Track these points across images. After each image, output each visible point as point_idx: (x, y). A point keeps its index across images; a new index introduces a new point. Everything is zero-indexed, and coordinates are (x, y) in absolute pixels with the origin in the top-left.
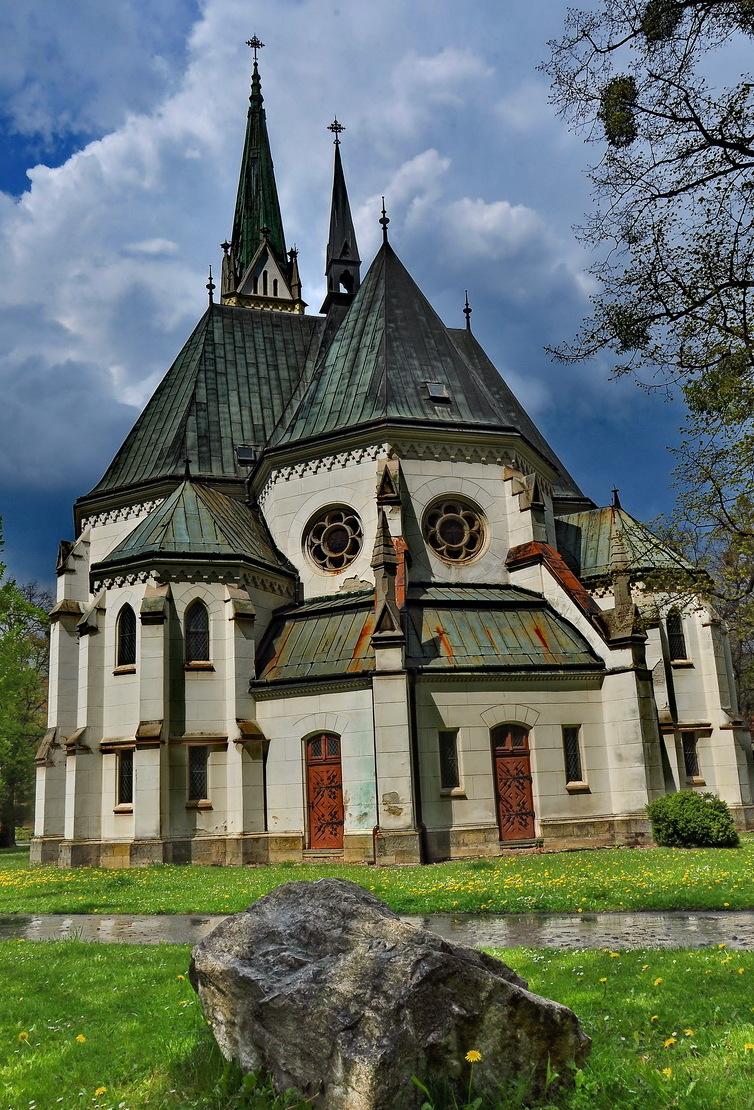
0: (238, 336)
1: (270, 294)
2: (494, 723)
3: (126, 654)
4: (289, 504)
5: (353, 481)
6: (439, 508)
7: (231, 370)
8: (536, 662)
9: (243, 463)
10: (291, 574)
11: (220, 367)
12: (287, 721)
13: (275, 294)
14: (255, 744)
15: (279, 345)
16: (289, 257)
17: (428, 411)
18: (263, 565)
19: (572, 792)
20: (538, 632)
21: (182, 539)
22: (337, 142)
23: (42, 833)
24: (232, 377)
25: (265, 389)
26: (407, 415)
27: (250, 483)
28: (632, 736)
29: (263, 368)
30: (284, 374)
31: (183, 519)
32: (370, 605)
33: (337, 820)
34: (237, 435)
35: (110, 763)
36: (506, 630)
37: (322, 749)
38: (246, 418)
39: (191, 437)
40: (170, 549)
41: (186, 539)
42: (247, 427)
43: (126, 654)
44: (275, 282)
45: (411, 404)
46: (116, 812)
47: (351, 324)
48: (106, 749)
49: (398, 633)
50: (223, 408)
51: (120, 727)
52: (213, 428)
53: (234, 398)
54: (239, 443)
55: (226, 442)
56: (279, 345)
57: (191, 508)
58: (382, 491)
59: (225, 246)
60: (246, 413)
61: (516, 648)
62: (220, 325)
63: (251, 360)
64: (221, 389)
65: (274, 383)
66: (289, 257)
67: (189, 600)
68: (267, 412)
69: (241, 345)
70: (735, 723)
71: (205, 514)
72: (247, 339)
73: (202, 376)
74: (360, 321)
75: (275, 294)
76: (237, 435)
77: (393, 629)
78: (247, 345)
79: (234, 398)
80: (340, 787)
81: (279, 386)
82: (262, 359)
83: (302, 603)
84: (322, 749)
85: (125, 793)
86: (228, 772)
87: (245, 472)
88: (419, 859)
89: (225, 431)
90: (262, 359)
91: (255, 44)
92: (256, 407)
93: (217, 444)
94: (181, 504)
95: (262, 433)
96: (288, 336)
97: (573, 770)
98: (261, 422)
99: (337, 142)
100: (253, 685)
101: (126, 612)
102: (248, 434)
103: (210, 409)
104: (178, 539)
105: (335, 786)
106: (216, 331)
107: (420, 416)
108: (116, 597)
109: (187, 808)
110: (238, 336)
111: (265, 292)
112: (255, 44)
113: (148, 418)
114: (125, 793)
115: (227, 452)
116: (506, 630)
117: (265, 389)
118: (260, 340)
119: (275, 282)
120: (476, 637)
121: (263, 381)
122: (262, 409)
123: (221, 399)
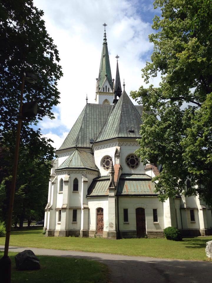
0: (93, 111)
1: (107, 92)
2: (136, 208)
3: (61, 189)
4: (99, 154)
5: (110, 151)
6: (130, 156)
7: (90, 120)
8: (147, 193)
9: (91, 143)
10: (98, 171)
11: (88, 119)
12: (93, 205)
13: (109, 91)
14: (87, 209)
15: (102, 113)
16: (113, 81)
17: (128, 134)
18: (93, 170)
19: (155, 224)
20: (149, 186)
21: (74, 165)
22: (117, 61)
23: (83, 229)
24: (90, 122)
25: (98, 124)
26: (123, 136)
27: (92, 148)
28: (168, 212)
29: (97, 119)
30: (102, 120)
31: (74, 159)
32: (109, 179)
33: (102, 228)
34: (90, 136)
35: (57, 213)
36: (142, 186)
37: (100, 211)
38: (93, 132)
39: (80, 137)
40: (70, 167)
41: (74, 164)
42: (93, 134)
43: (61, 189)
44: (109, 88)
45: (125, 133)
46: (124, 224)
47: (114, 112)
48: (56, 210)
49: (114, 188)
50: (88, 130)
51: (59, 206)
52: (85, 135)
53: (90, 127)
54: (90, 138)
55: (88, 138)
56: (102, 113)
57: (76, 156)
58: (116, 154)
59: (97, 79)
60: (93, 130)
61: (143, 190)
62: (89, 109)
63: (95, 117)
64: (88, 125)
65: (100, 123)
66: (113, 81)
67: (74, 178)
68: (97, 130)
69: (93, 113)
70: (203, 208)
71: (79, 158)
72: (94, 112)
73: (83, 122)
74: (116, 111)
75: (109, 91)
76: (90, 136)
77: (113, 187)
78: (95, 113)
79: (90, 127)
80: (103, 220)
81: (101, 123)
82: (97, 117)
83: (100, 177)
84: (100, 211)
85: (60, 220)
86: (82, 216)
87: (91, 145)
88: (116, 238)
89: (88, 135)
90: (97, 117)
91: (105, 25)
92: (95, 129)
93: (86, 139)
94: (74, 155)
95: (96, 135)
96: (104, 110)
97: (155, 219)
98: (96, 133)
99: (117, 61)
100: (87, 197)
101: (62, 180)
102: (93, 136)
103: (85, 130)
104: (73, 164)
105: (102, 220)
106: (87, 110)
107: (126, 136)
108: (60, 177)
109: (72, 223)
110: (93, 111)
111: (106, 91)
112: (105, 25)
113: (66, 141)
114: (60, 220)
115: (88, 141)
116: (142, 186)
117: (98, 124)
118: (97, 111)
119: (109, 88)
120: (134, 187)
121: (97, 122)
122: (97, 129)
123: (87, 128)
